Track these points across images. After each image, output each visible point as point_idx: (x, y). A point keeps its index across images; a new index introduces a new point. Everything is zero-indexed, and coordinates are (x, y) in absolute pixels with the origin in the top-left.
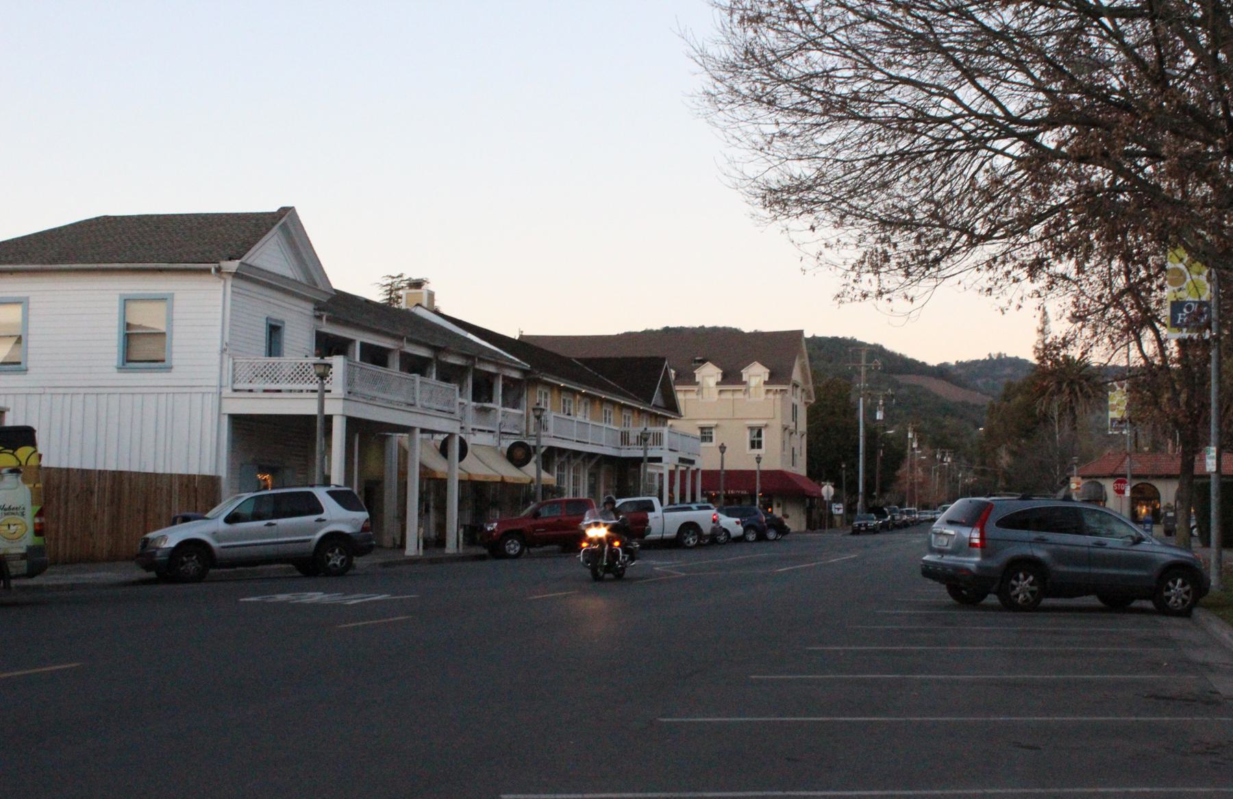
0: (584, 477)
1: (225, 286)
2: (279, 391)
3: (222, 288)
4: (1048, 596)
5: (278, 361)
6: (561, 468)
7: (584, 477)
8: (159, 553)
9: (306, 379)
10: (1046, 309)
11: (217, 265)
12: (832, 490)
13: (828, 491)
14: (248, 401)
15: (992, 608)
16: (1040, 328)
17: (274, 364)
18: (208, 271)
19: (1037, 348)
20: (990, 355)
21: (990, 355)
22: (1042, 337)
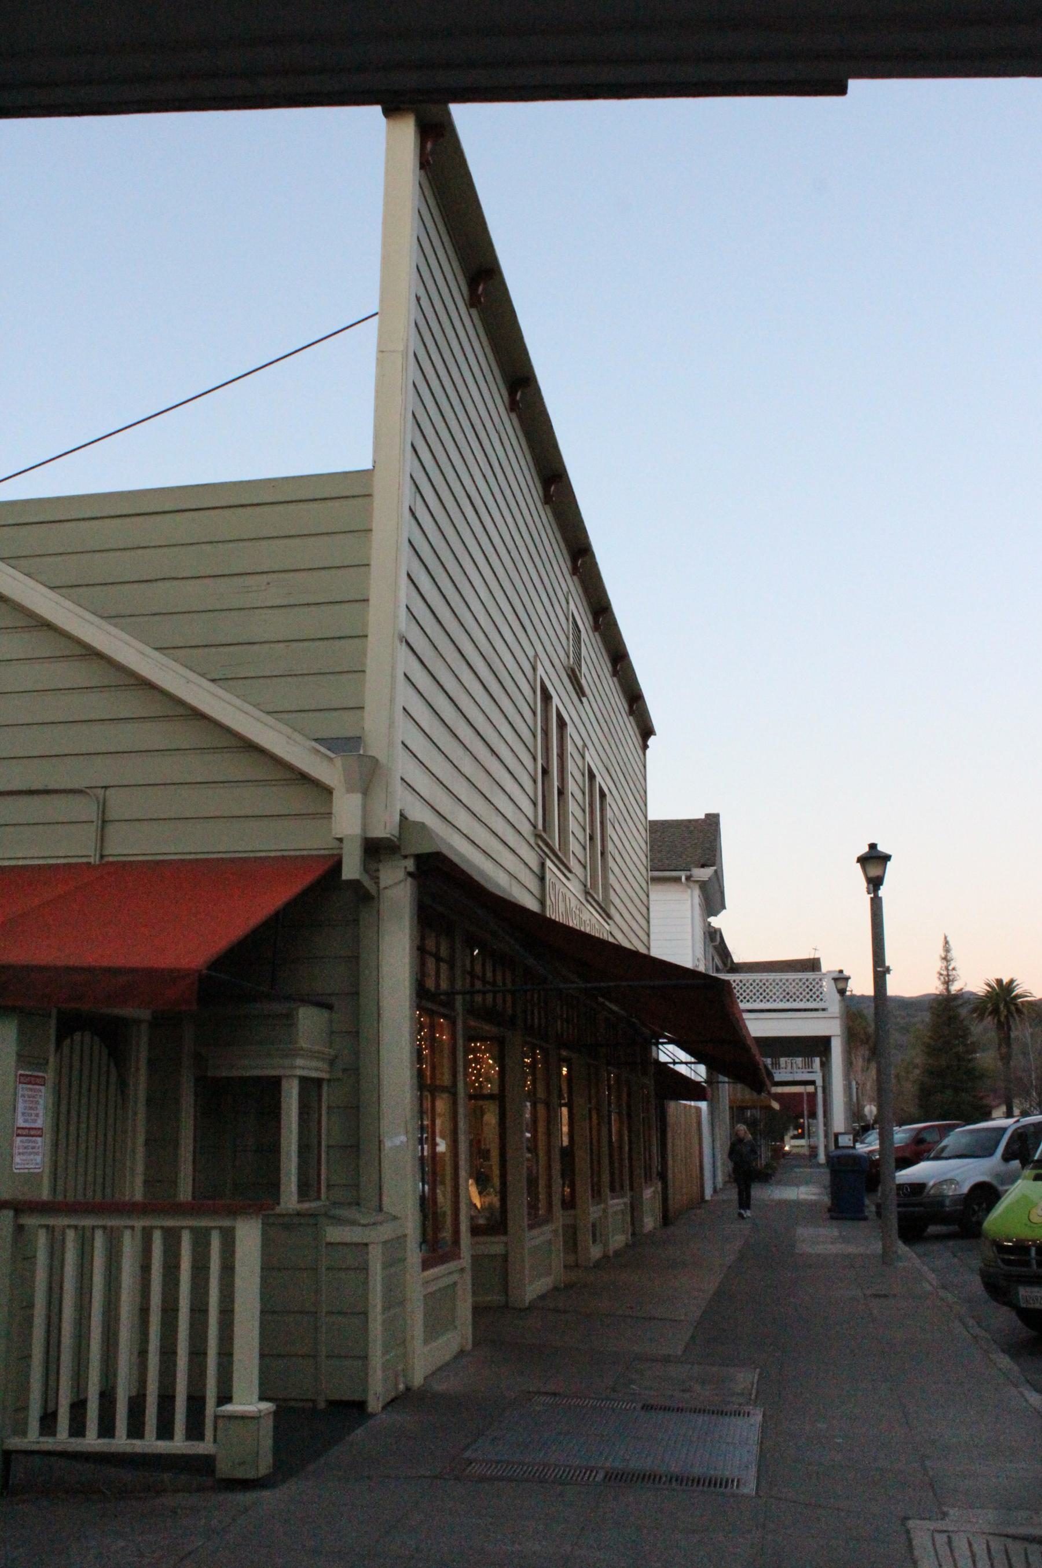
0: (317, 1069)
1: (692, 897)
2: (816, 1010)
3: (690, 899)
4: (38, 1173)
5: (813, 977)
6: (982, 1098)
7: (317, 1069)
8: (947, 1202)
9: (814, 996)
10: (948, 939)
11: (688, 873)
12: (874, 1109)
13: (871, 1112)
14: (793, 1021)
15: (1030, 1241)
16: (943, 956)
17: (807, 980)
18: (677, 880)
19: (941, 974)
20: (989, 985)
21: (1012, 981)
22: (945, 964)
